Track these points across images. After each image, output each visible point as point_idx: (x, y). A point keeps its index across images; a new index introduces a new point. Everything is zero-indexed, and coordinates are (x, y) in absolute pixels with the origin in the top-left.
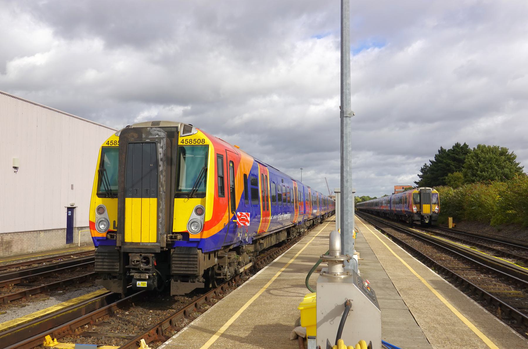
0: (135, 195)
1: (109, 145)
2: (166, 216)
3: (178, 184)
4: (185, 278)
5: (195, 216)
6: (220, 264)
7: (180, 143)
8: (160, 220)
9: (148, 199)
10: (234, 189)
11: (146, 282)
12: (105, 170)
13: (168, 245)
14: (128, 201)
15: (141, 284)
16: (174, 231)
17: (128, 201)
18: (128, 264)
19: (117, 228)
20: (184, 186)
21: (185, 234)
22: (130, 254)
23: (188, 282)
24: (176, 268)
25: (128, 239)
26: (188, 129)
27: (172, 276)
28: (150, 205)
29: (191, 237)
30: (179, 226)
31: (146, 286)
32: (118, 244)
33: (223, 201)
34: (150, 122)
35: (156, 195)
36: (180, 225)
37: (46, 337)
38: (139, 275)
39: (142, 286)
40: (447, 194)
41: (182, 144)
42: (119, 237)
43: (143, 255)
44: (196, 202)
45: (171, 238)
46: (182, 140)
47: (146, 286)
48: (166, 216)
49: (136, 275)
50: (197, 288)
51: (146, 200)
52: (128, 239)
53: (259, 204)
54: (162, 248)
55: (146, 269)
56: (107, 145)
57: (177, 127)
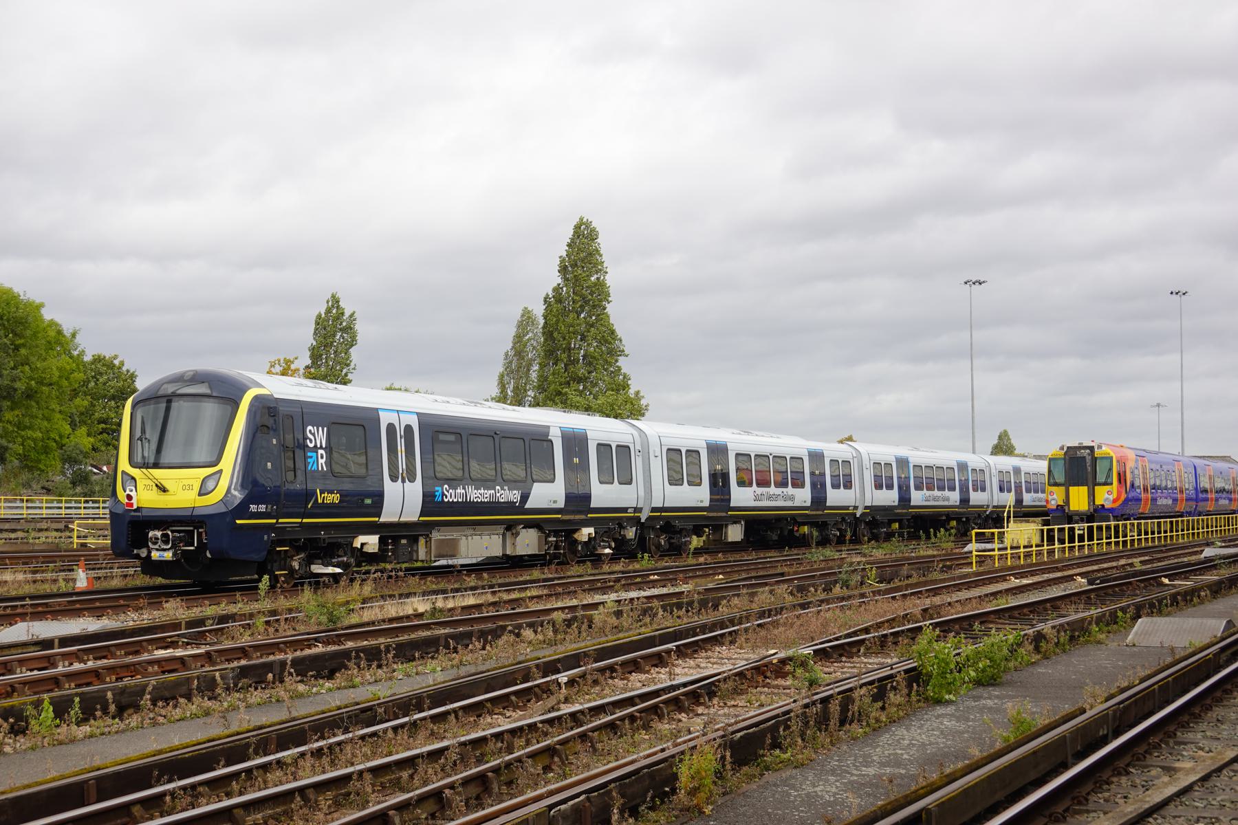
2: (1092, 495)
26: (1100, 447)
28: (1084, 490)
44: (1107, 488)
46: (1097, 453)
48: (1092, 495)
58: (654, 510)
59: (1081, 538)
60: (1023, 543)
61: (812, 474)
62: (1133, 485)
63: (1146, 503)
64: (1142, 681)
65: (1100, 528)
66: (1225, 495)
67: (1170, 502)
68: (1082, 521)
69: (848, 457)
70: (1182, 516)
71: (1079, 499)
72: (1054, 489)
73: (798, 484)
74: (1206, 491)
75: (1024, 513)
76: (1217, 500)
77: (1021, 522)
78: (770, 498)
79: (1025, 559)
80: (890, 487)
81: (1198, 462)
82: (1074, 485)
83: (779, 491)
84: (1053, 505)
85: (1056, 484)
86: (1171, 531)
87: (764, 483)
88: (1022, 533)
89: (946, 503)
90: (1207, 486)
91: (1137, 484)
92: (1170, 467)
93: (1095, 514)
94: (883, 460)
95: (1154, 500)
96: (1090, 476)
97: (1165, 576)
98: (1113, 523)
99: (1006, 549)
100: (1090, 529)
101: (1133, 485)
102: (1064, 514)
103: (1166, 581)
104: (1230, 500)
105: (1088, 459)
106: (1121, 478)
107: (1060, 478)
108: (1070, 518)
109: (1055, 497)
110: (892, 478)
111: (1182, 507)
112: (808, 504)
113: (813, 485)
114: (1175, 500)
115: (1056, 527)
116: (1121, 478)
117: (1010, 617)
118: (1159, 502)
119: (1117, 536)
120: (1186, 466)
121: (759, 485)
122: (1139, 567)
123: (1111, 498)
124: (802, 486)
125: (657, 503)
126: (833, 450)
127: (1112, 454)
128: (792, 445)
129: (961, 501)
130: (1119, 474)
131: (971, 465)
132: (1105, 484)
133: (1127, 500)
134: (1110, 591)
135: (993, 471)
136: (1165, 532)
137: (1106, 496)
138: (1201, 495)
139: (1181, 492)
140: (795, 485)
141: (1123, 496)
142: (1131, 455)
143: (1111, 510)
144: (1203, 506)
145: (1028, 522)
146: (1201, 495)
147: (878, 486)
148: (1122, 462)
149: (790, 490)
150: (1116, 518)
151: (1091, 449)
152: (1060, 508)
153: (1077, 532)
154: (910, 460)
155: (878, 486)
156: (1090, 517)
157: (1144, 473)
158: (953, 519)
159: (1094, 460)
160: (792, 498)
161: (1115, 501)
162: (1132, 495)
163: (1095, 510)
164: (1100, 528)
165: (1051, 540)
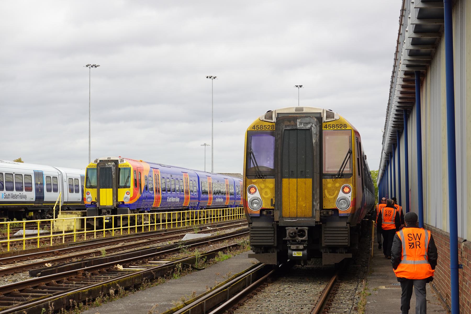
1: (256, 130)
2: (116, 195)
3: (119, 183)
5: (126, 195)
9: (105, 189)
10: (141, 184)
11: (301, 252)
13: (117, 206)
14: (101, 189)
15: (296, 254)
16: (324, 208)
17: (101, 189)
20: (121, 184)
21: (123, 202)
22: (287, 228)
23: (337, 253)
25: (101, 204)
26: (122, 161)
28: (110, 191)
34: (294, 108)
36: (120, 199)
39: (297, 255)
40: (375, 182)
43: (299, 228)
44: (126, 190)
46: (120, 165)
48: (116, 195)
49: (293, 247)
50: (345, 258)
51: (108, 189)
52: (101, 204)
54: (316, 222)
55: (302, 241)
56: (253, 130)
58: (65, 202)
59: (109, 225)
60: (64, 229)
61: (36, 184)
62: (146, 188)
63: (158, 202)
64: (246, 271)
65: (125, 218)
66: (220, 195)
67: (178, 200)
68: (108, 213)
69: (56, 174)
70: (188, 209)
71: (106, 198)
72: (90, 190)
73: (29, 189)
74: (206, 193)
75: (68, 207)
76: (214, 199)
77: (67, 213)
78: (13, 197)
79: (168, 227)
80: (77, 191)
81: (198, 173)
82: (103, 187)
83: (18, 193)
84: (88, 201)
85: (91, 187)
86: (223, 215)
87: (10, 189)
88: (66, 222)
89: (24, 200)
90: (208, 189)
91: (150, 186)
92: (178, 177)
93: (118, 208)
94: (74, 177)
95: (164, 199)
96: (114, 181)
97: (120, 263)
98: (129, 215)
99: (49, 233)
100: (117, 219)
101: (146, 188)
102: (97, 209)
103: (120, 267)
104: (225, 199)
105: (113, 169)
106: (137, 183)
107: (94, 182)
108: (100, 211)
109: (91, 196)
110: (78, 186)
111: (187, 203)
112: (34, 200)
113: (37, 190)
114: (182, 199)
115: (121, 215)
116: (137, 183)
117: (137, 263)
118: (169, 200)
119: (196, 218)
120: (191, 176)
121: (7, 189)
122: (104, 255)
123: (129, 197)
124: (31, 190)
125: (66, 200)
126: (48, 170)
127: (130, 166)
128: (27, 168)
129: (36, 198)
130: (135, 180)
131: (46, 174)
132: (125, 187)
133: (140, 199)
134: (104, 270)
135: (65, 178)
136: (220, 216)
137: (125, 195)
138: (202, 196)
139: (187, 193)
140: (27, 190)
141: (138, 196)
142: (146, 167)
143: (128, 206)
144: (202, 203)
145: (71, 213)
146: (202, 196)
147: (71, 191)
148: (138, 172)
149: (24, 193)
150: (133, 211)
151: (116, 162)
152: (93, 204)
153: (105, 221)
154: (44, 173)
155: (71, 191)
156: (114, 211)
157: (187, 182)
158: (31, 211)
159: (118, 170)
160: (25, 197)
161: (131, 199)
162: (145, 194)
163: (118, 206)
164: (125, 218)
165: (90, 227)
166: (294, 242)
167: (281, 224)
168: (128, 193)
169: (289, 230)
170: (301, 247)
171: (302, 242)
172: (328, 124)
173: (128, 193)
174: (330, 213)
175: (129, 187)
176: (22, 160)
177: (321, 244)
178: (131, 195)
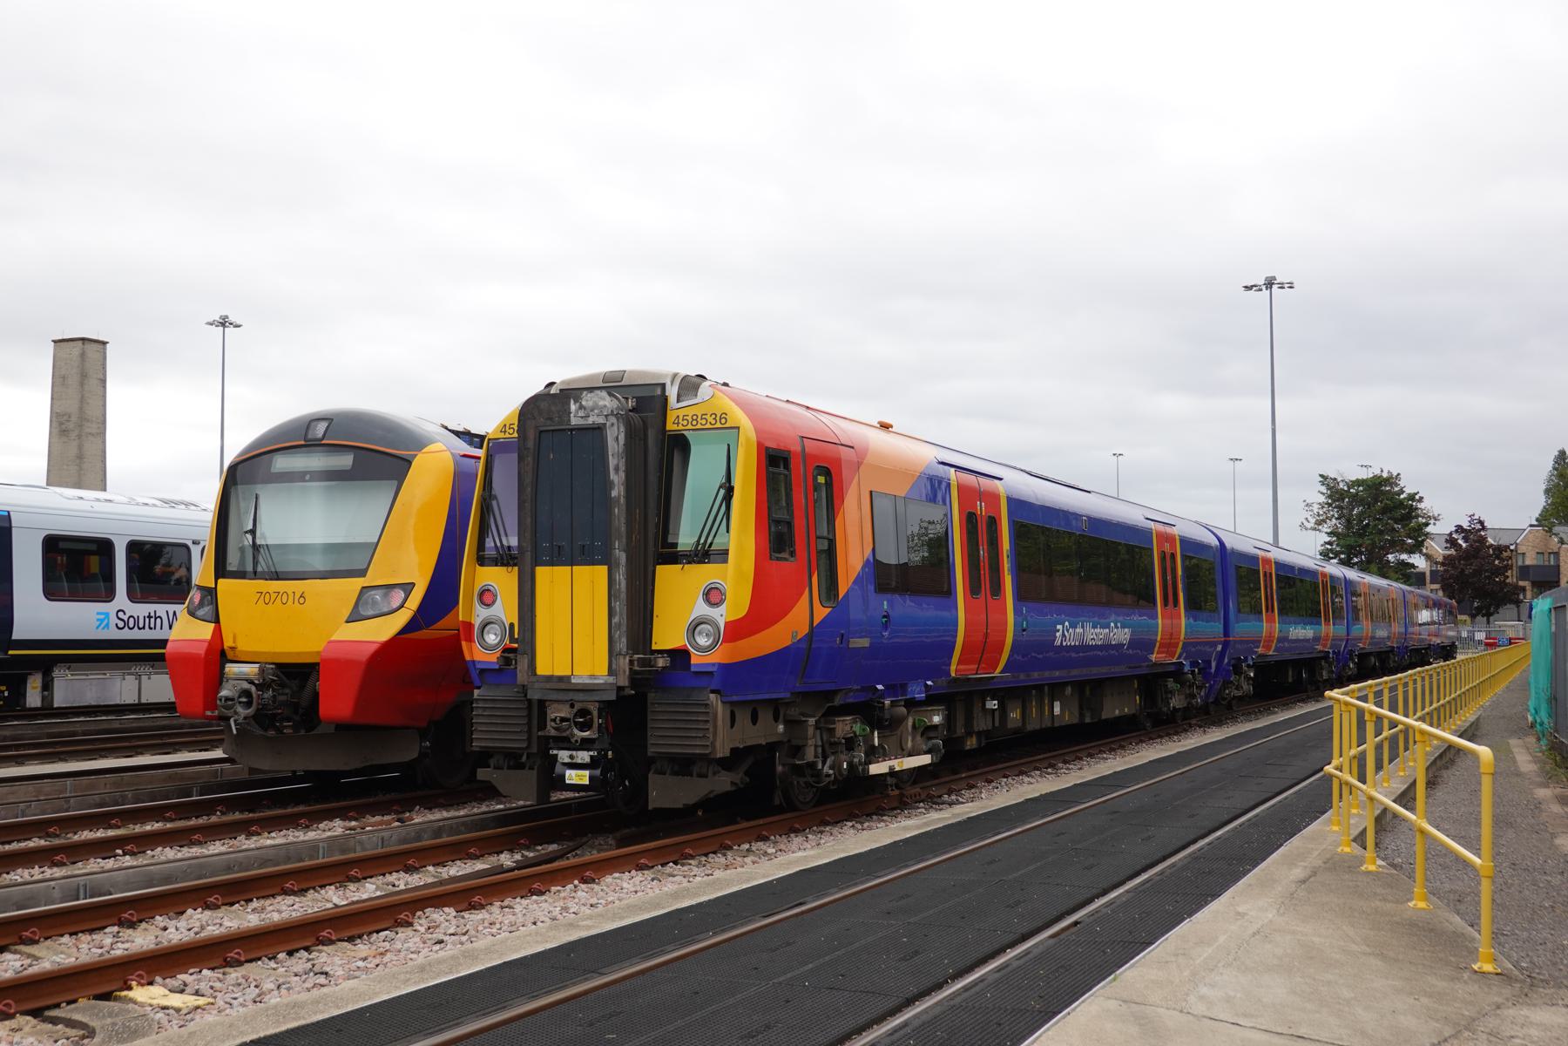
0: (560, 557)
2: (635, 610)
4: (684, 765)
5: (701, 609)
6: (794, 742)
7: (670, 426)
8: (616, 620)
9: (564, 571)
11: (587, 773)
12: (495, 497)
14: (541, 571)
16: (654, 647)
17: (541, 571)
18: (542, 726)
19: (516, 641)
20: (686, 538)
21: (680, 656)
24: (660, 741)
25: (543, 668)
27: (651, 761)
29: (696, 659)
30: (667, 636)
31: (586, 781)
32: (522, 677)
33: (787, 567)
35: (606, 559)
36: (667, 636)
37: (39, 704)
38: (567, 753)
41: (675, 427)
42: (522, 664)
44: (706, 574)
45: (642, 662)
47: (586, 781)
49: (564, 756)
52: (543, 668)
53: (1279, 588)
54: (620, 689)
57: (663, 386)
123: (722, 615)
132: (703, 554)
137: (698, 608)
161: (736, 631)
166: (566, 743)
167: (535, 695)
168: (713, 596)
169: (557, 712)
170: (584, 756)
171: (585, 744)
172: (681, 413)
173: (487, 598)
174: (661, 663)
175: (723, 555)
176: (232, 319)
177: (24, 695)
178: (735, 606)
